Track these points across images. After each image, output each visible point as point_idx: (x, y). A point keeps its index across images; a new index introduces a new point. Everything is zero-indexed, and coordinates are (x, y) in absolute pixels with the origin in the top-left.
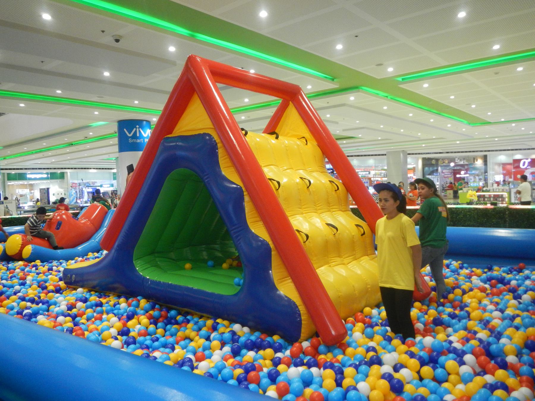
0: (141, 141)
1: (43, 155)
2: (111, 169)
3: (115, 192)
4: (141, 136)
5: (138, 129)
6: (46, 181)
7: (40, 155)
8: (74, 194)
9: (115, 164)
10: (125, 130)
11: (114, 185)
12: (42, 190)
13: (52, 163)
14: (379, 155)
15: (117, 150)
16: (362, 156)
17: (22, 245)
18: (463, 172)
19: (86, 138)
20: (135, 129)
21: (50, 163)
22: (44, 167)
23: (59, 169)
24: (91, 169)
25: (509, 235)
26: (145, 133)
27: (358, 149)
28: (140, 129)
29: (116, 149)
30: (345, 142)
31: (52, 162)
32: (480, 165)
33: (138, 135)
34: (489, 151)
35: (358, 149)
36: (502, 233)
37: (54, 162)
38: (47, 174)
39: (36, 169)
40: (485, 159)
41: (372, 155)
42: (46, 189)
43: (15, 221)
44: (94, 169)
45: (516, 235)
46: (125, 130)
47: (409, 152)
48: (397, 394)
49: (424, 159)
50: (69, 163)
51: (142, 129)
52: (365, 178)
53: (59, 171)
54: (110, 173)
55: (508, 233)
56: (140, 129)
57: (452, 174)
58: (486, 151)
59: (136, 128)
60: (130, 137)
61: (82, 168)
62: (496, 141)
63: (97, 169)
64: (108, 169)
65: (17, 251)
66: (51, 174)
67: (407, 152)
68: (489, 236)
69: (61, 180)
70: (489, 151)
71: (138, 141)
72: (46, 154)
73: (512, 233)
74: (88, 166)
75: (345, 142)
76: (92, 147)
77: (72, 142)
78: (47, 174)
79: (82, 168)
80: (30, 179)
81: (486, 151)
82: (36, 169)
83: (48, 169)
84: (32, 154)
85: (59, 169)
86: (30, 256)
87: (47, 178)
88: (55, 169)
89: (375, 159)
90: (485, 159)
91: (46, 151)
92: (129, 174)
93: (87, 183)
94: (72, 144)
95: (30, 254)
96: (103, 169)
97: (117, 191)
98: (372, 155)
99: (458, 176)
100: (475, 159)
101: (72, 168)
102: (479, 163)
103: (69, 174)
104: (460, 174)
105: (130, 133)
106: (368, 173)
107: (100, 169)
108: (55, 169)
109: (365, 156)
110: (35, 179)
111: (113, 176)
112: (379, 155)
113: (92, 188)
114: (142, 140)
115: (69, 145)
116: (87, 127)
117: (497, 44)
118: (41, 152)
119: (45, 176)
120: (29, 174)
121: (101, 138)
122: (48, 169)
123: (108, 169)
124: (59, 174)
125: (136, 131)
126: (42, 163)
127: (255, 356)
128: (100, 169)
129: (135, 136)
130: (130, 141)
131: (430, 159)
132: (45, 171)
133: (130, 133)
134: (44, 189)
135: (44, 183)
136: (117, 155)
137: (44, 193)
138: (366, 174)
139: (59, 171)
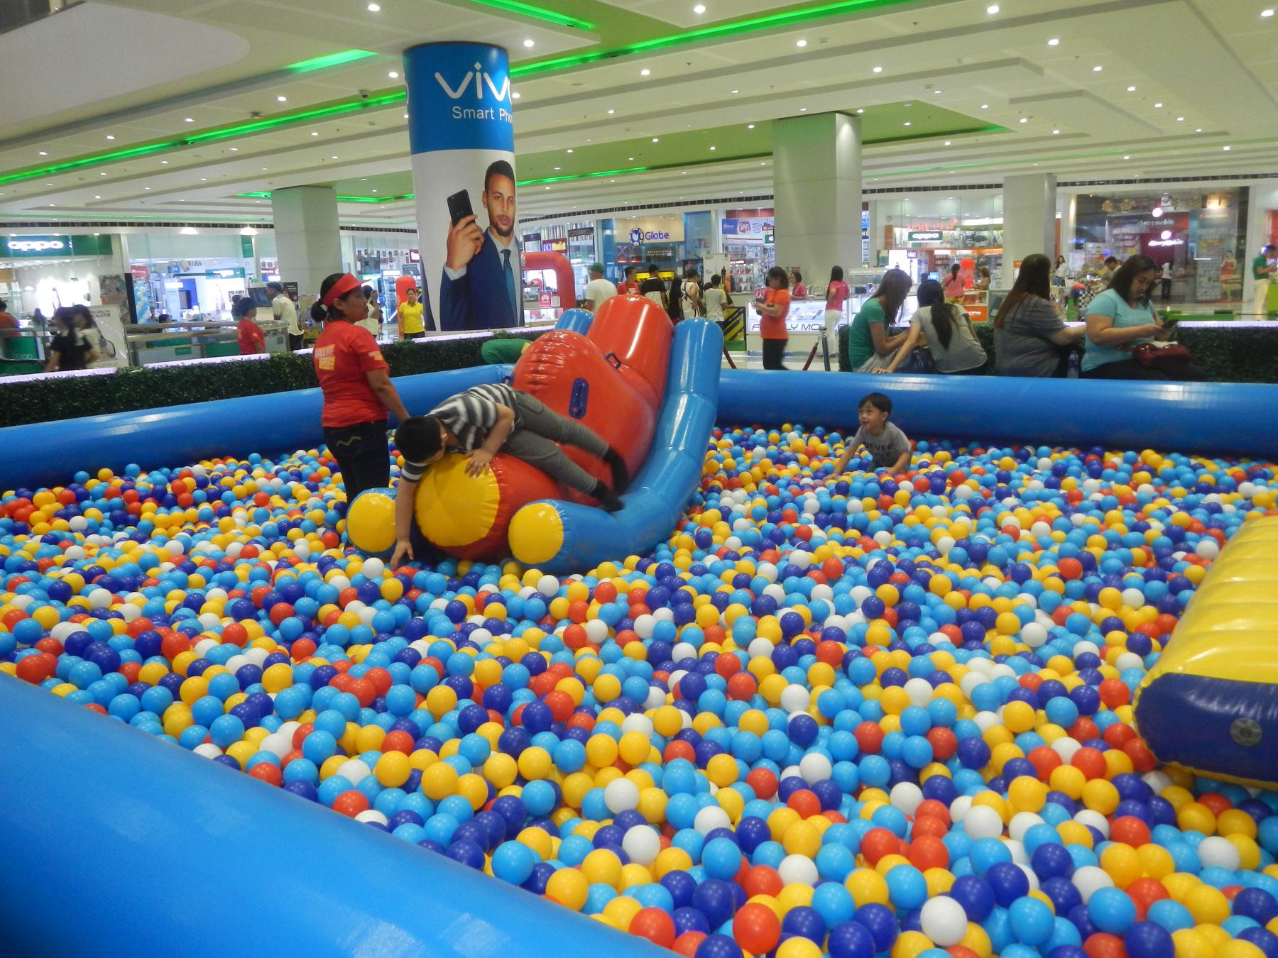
0: (489, 114)
1: (372, 124)
2: (237, 226)
3: (291, 288)
4: (489, 100)
5: (479, 75)
6: (60, 261)
7: (72, 178)
8: (144, 294)
9: (270, 210)
10: (438, 76)
11: (247, 272)
12: (108, 282)
13: (90, 207)
14: (972, 187)
15: (408, 148)
16: (926, 189)
17: (502, 502)
18: (1166, 235)
19: (256, 114)
20: (470, 75)
21: (82, 205)
22: (55, 220)
23: (95, 224)
24: (182, 225)
25: (926, 387)
26: (499, 91)
27: (938, 169)
28: (486, 75)
29: (403, 141)
30: (948, 143)
31: (88, 204)
32: (1219, 216)
33: (480, 96)
34: (1255, 176)
35: (938, 169)
36: (1174, 392)
37: (98, 203)
38: (64, 239)
39: (32, 225)
40: (1240, 200)
41: (954, 188)
42: (123, 278)
43: (214, 379)
44: (191, 225)
45: (1194, 397)
46: (438, 76)
47: (1061, 179)
48: (679, 689)
49: (1082, 199)
50: (143, 206)
51: (491, 76)
52: (922, 251)
53: (96, 232)
54: (235, 237)
55: (1199, 392)
56: (486, 75)
57: (1137, 238)
58: (1246, 177)
59: (475, 71)
60: (455, 102)
61: (159, 225)
62: (1126, 161)
63: (199, 225)
64: (230, 226)
65: (484, 533)
66: (76, 239)
67: (1056, 178)
68: (1151, 401)
69: (102, 257)
70: (1255, 176)
71: (482, 114)
72: (89, 175)
73: (1213, 393)
74: (215, 219)
75: (948, 143)
76: (179, 164)
77: (184, 134)
78: (64, 239)
79: (159, 225)
80: (19, 254)
81: (1246, 177)
82: (32, 225)
83: (65, 224)
84: (48, 174)
85: (95, 224)
86: (560, 553)
87: (64, 253)
88: (84, 224)
89: (960, 198)
90: (1240, 200)
91: (93, 167)
92: (455, 222)
93: (177, 266)
94: (185, 143)
95: (558, 548)
96: (215, 225)
97: (295, 284)
98: (954, 188)
99: (1153, 243)
100: (1204, 199)
101: (131, 224)
102: (1216, 208)
103: (124, 240)
104: (1158, 238)
105: (455, 89)
106: (914, 236)
107: (207, 225)
108: (84, 224)
109: (936, 188)
110: (33, 254)
111: (243, 248)
112: (972, 187)
113: (182, 281)
114: (492, 111)
115: (174, 145)
116: (278, 75)
117: (391, 78)
118: (76, 168)
119: (60, 245)
120: (14, 239)
121: (284, 122)
122: (65, 224)
123: (230, 226)
124: (96, 239)
125: (473, 82)
126: (60, 206)
127: (377, 615)
128: (207, 225)
129: (470, 99)
130: (457, 113)
131: (1099, 200)
132: (57, 232)
133: (455, 89)
134: (117, 277)
135: (53, 265)
136: (405, 165)
137: (117, 289)
138: (923, 239)
139: (96, 232)
